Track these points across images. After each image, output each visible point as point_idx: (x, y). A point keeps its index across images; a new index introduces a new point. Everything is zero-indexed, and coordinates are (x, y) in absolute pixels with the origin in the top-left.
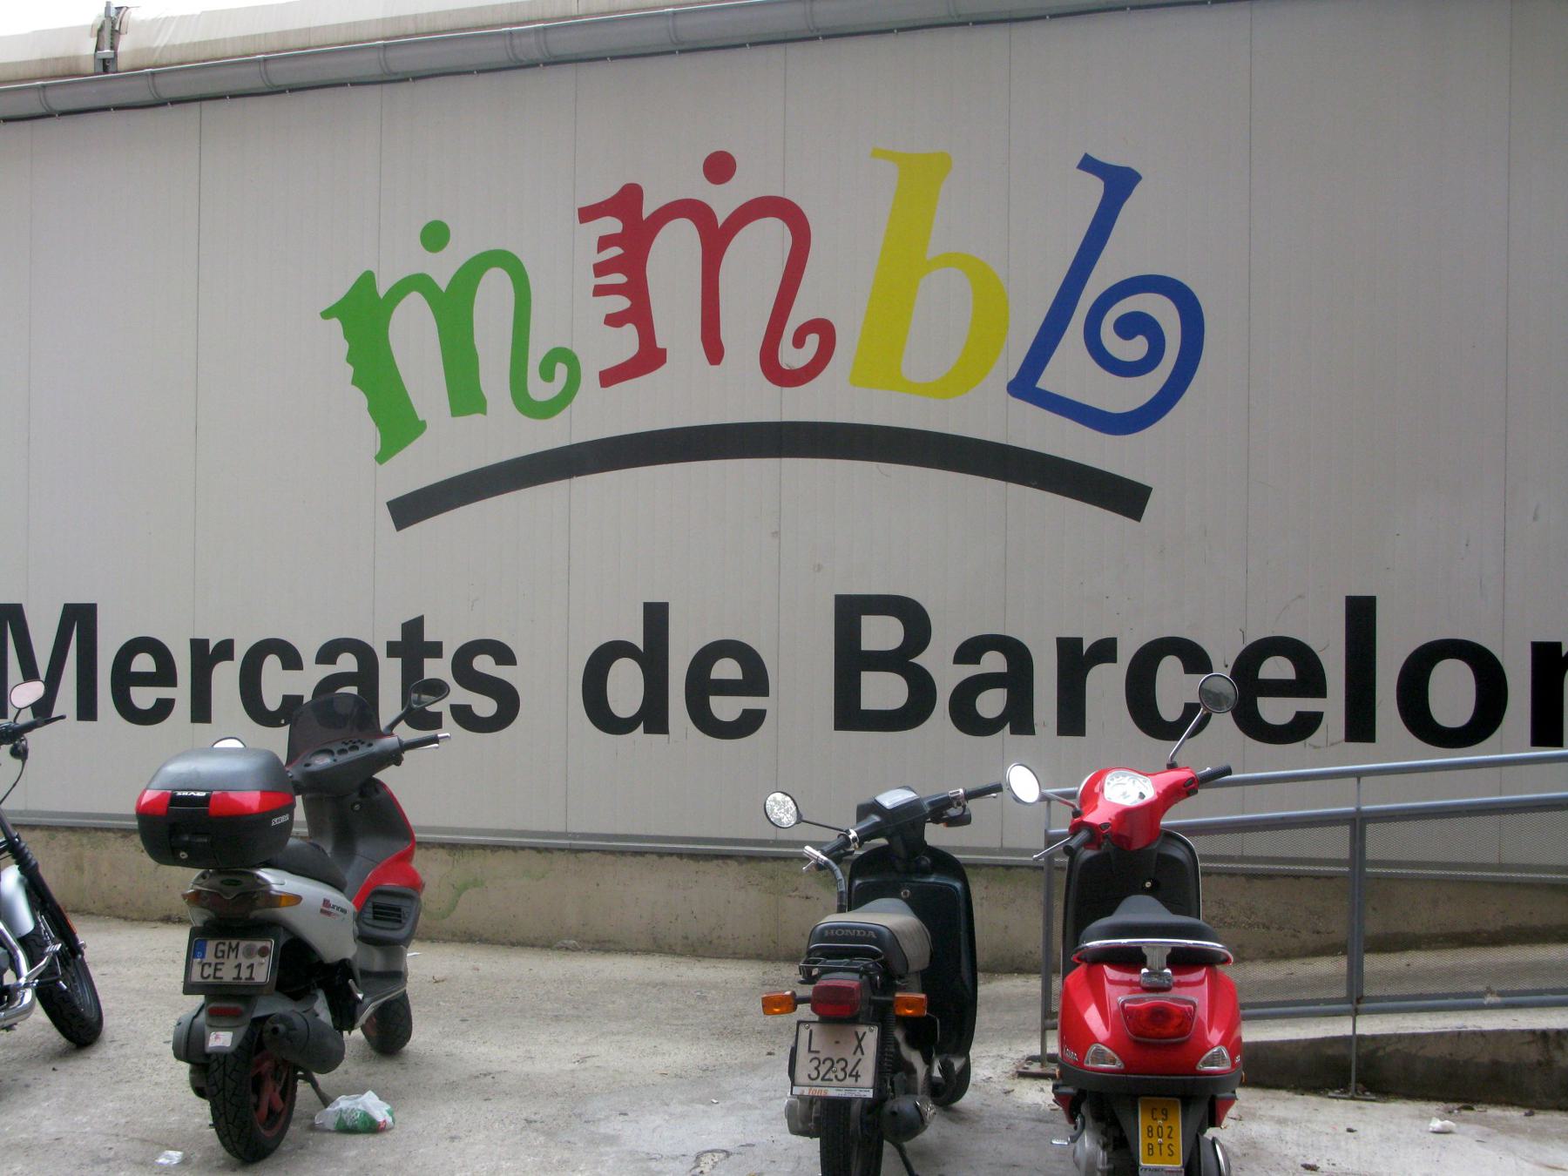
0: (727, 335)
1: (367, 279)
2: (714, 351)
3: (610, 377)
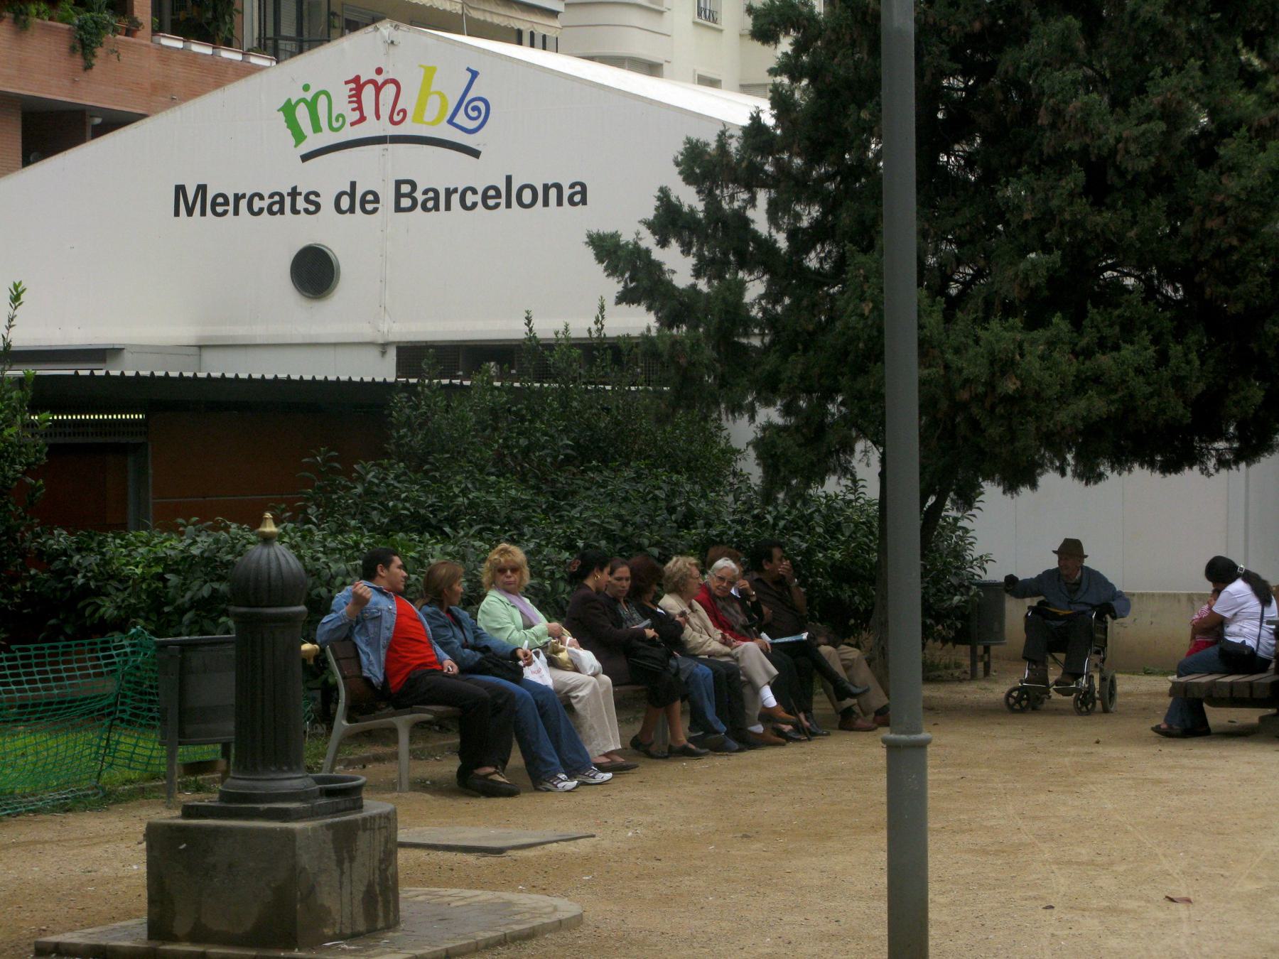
0: (381, 113)
1: (289, 101)
2: (378, 117)
3: (353, 124)
